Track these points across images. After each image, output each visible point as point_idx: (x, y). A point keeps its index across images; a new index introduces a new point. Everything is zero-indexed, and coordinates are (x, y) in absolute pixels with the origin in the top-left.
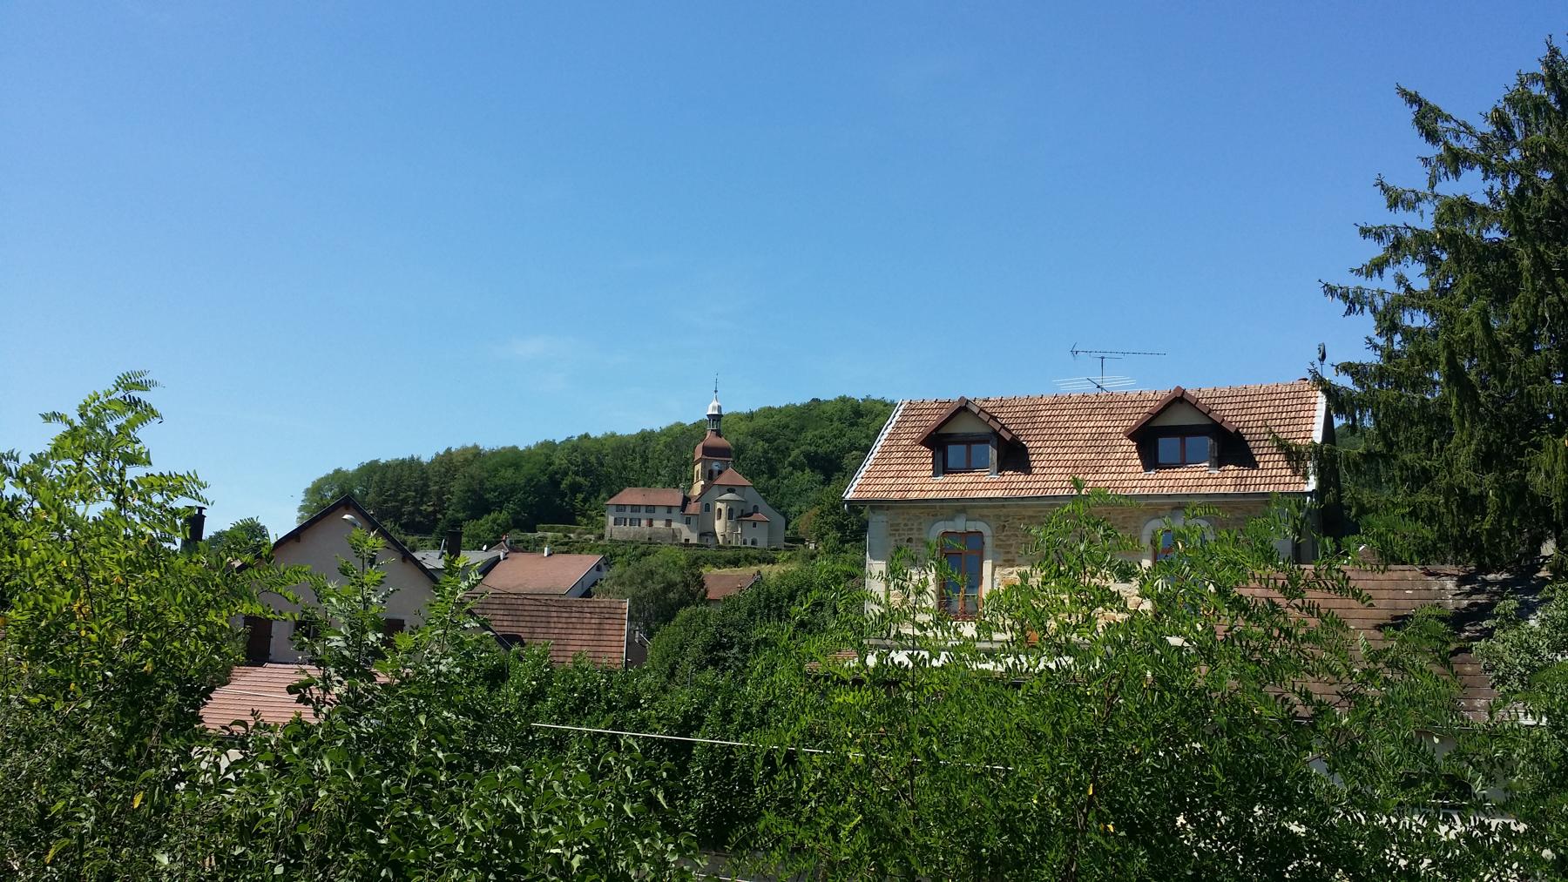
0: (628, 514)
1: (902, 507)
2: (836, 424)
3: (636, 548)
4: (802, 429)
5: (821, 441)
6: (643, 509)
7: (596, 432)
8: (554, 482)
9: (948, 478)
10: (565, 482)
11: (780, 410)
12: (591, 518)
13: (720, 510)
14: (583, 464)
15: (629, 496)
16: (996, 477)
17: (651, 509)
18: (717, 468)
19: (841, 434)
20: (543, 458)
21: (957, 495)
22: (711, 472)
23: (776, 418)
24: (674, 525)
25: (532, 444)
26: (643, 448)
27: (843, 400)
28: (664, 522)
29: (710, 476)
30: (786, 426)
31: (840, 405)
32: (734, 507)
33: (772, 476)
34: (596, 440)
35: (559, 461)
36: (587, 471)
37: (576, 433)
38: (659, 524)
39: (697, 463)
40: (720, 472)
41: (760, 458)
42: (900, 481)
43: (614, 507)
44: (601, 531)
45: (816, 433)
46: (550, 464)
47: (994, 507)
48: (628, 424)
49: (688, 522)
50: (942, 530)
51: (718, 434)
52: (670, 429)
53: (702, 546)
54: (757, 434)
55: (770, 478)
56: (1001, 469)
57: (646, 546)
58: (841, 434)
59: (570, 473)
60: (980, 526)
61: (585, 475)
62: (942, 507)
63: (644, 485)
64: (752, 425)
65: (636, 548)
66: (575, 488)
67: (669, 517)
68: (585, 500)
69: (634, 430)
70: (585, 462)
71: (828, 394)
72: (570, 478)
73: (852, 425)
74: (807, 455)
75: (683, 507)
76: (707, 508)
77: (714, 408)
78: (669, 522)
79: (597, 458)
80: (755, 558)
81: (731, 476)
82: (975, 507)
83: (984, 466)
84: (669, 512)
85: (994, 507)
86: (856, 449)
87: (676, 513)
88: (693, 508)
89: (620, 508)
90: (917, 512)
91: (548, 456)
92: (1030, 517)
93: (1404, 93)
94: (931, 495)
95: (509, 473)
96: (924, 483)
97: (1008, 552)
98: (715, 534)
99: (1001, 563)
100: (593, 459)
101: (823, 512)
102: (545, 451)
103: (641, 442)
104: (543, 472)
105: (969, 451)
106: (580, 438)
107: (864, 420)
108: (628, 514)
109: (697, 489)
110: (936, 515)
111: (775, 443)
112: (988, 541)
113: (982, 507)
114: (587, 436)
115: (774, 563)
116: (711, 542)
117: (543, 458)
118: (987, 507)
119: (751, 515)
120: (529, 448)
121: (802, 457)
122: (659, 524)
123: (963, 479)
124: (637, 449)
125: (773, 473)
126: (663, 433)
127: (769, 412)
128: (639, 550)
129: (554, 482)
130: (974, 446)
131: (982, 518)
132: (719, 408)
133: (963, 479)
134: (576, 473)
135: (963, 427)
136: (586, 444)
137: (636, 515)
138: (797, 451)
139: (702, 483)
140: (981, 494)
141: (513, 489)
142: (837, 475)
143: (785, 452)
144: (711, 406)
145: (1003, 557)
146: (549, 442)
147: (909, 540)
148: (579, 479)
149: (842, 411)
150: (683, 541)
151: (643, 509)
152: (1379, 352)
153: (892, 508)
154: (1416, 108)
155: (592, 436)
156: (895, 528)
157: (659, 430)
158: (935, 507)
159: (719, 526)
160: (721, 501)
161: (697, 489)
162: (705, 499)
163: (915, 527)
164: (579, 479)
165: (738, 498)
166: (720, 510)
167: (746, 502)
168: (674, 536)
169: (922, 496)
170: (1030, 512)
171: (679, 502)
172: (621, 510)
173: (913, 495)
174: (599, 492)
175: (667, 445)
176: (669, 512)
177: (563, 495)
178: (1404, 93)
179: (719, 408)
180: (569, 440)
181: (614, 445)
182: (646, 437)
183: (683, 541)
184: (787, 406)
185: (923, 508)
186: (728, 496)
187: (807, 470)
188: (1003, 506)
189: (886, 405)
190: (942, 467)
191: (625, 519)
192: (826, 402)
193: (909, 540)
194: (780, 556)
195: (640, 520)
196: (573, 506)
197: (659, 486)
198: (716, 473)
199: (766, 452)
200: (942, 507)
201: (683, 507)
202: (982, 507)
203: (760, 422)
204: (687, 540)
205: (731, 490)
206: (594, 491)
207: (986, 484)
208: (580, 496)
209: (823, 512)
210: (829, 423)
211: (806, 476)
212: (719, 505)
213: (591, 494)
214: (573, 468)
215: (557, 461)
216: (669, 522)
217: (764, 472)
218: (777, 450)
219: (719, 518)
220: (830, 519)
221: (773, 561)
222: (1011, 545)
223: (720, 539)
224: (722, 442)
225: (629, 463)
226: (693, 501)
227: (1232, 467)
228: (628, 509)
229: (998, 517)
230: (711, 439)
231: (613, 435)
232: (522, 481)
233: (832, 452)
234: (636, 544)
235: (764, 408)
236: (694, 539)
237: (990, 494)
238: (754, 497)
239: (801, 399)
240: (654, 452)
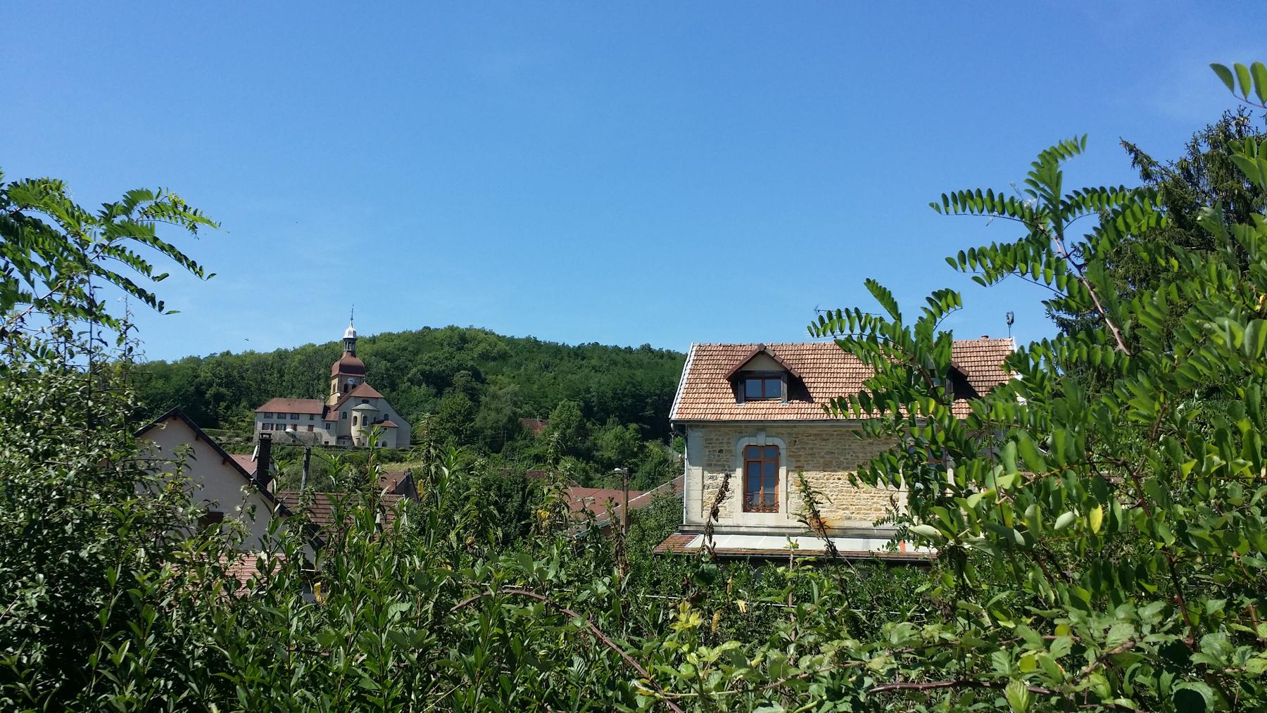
0: (275, 420)
1: (714, 426)
2: (447, 348)
3: (282, 449)
4: (417, 352)
5: (434, 362)
6: (288, 417)
7: (237, 350)
8: (200, 393)
9: (749, 405)
10: (209, 392)
11: (399, 336)
12: (232, 423)
13: (356, 418)
14: (226, 377)
15: (275, 405)
16: (787, 405)
17: (295, 416)
18: (351, 383)
19: (452, 357)
20: (190, 372)
21: (760, 417)
22: (346, 386)
23: (396, 342)
24: (316, 430)
25: (179, 359)
26: (280, 364)
27: (452, 328)
28: (307, 427)
29: (345, 389)
30: (405, 349)
31: (449, 333)
32: (368, 415)
33: (393, 390)
34: (237, 356)
35: (205, 374)
36: (229, 382)
37: (219, 350)
38: (302, 429)
39: (334, 377)
40: (354, 386)
41: (382, 374)
42: (712, 406)
43: (263, 415)
44: (248, 434)
45: (430, 355)
46: (196, 377)
47: (787, 427)
48: (266, 345)
49: (328, 427)
50: (747, 444)
51: (353, 354)
52: (303, 349)
53: (340, 447)
54: (382, 355)
55: (391, 391)
56: (790, 398)
57: (291, 448)
58: (452, 357)
59: (215, 385)
60: (777, 441)
61: (227, 386)
62: (746, 427)
63: (280, 396)
64: (375, 347)
65: (282, 449)
66: (219, 398)
67: (311, 423)
68: (227, 408)
69: (271, 350)
70: (228, 376)
71: (439, 322)
72: (214, 389)
73: (459, 349)
74: (423, 373)
75: (324, 415)
76: (345, 415)
77: (350, 333)
78: (311, 427)
79: (239, 372)
80: (386, 458)
81: (365, 390)
82: (772, 427)
83: (776, 396)
84: (312, 419)
85: (787, 427)
86: (464, 369)
87: (318, 419)
88: (332, 416)
89: (268, 415)
90: (726, 430)
91: (194, 370)
92: (815, 435)
93: (1126, 144)
94: (740, 418)
95: (160, 383)
96: (728, 408)
97: (799, 461)
98: (351, 438)
99: (793, 469)
100: (235, 373)
101: (442, 420)
102: (192, 365)
103: (277, 359)
104: (190, 383)
105: (763, 384)
106: (222, 355)
107: (470, 346)
108: (275, 420)
109: (333, 400)
110: (742, 433)
111: (396, 363)
112: (783, 452)
113: (778, 427)
114: (228, 353)
115: (402, 462)
116: (347, 444)
117: (190, 372)
118: (782, 427)
119: (382, 422)
120: (175, 363)
121: (419, 375)
122: (302, 429)
123: (762, 406)
124: (275, 366)
125: (393, 387)
126: (296, 352)
127: (389, 337)
128: (286, 451)
129: (200, 393)
130: (767, 381)
131: (777, 435)
132: (354, 332)
133: (762, 406)
134: (220, 385)
135: (762, 366)
136: (230, 360)
137: (281, 421)
138: (415, 370)
139: (339, 395)
140: (779, 417)
141: (164, 397)
142: (448, 389)
143: (403, 370)
144: (347, 331)
145: (794, 464)
146: (194, 358)
147: (721, 451)
148: (223, 390)
149: (451, 337)
150: (323, 443)
151: (288, 417)
152: (1055, 321)
153: (707, 427)
154: (1133, 155)
155: (234, 353)
156: (708, 441)
157: (292, 349)
158: (741, 426)
159: (354, 431)
160: (357, 410)
161: (333, 400)
162: (343, 408)
163: (725, 441)
164: (223, 390)
165: (371, 408)
166: (356, 418)
167: (378, 411)
168: (316, 439)
169: (733, 417)
170: (815, 431)
171: (321, 411)
172: (269, 417)
173: (726, 417)
174: (240, 400)
175: (301, 362)
176: (312, 419)
177: (207, 403)
178: (1126, 144)
179: (354, 332)
180: (212, 356)
181: (254, 361)
182: (281, 355)
183: (323, 443)
184: (404, 332)
185: (732, 427)
186: (363, 406)
187: (424, 385)
188: (795, 427)
189: (486, 334)
190: (741, 397)
191: (272, 425)
192: (436, 330)
193: (721, 451)
194: (408, 456)
195: (285, 425)
196: (216, 413)
197: (294, 396)
198: (350, 387)
199: (387, 370)
200: (746, 427)
201: (324, 415)
202: (778, 427)
203: (381, 345)
204: (327, 442)
205: (365, 401)
206: (236, 401)
207: (779, 410)
208: (223, 404)
209: (442, 420)
210: (439, 347)
211: (422, 390)
212: (355, 414)
213: (232, 403)
214: (217, 380)
215: (202, 374)
216: (311, 427)
217: (386, 387)
218: (397, 368)
219: (355, 424)
220: (448, 425)
221: (401, 460)
222: (801, 455)
223: (355, 441)
224: (358, 361)
225: (268, 377)
226: (332, 409)
227: (963, 400)
228: (275, 416)
229: (789, 434)
230: (346, 358)
231: (252, 353)
232: (172, 392)
233: (444, 371)
234: (284, 446)
235: (385, 334)
236: (333, 442)
237: (786, 417)
238: (385, 407)
239: (416, 327)
240: (290, 368)
